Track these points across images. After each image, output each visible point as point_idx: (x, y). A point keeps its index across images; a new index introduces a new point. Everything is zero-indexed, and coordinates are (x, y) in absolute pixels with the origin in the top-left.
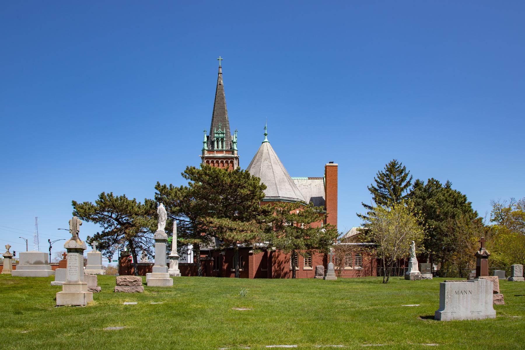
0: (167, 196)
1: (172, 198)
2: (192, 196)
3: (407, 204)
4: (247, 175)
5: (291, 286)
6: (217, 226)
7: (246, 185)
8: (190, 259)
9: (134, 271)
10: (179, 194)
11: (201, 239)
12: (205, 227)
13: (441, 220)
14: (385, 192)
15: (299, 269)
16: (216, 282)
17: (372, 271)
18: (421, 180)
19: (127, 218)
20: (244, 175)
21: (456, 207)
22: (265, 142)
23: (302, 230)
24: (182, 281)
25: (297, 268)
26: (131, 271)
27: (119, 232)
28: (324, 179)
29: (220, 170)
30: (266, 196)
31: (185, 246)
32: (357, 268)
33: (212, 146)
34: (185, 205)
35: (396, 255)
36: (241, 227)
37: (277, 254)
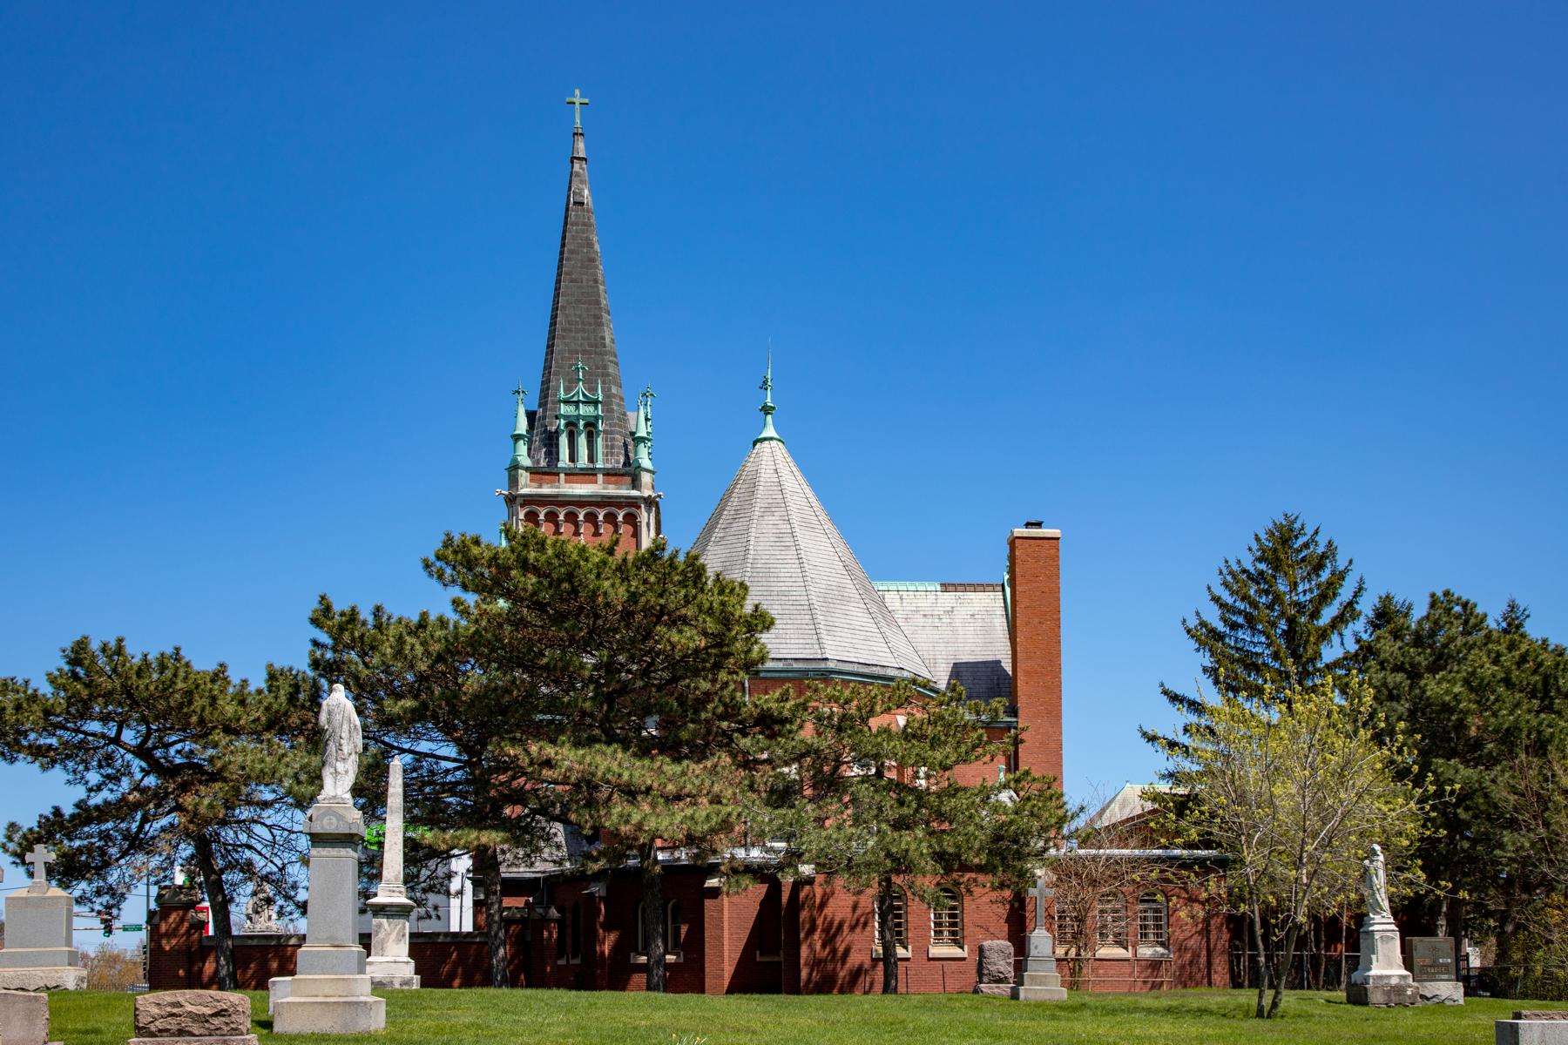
0: (362, 655)
1: (384, 663)
2: (468, 654)
3: (1347, 694)
4: (694, 572)
5: (878, 1027)
6: (573, 779)
7: (690, 611)
8: (460, 916)
9: (217, 972)
10: (413, 646)
11: (505, 830)
12: (522, 780)
13: (1491, 762)
14: (1255, 645)
15: (909, 955)
16: (570, 1009)
17: (1209, 964)
18: (1399, 599)
19: (188, 746)
20: (683, 573)
21: (1548, 708)
22: (765, 439)
23: (920, 795)
24: (425, 1008)
25: (900, 952)
26: (201, 971)
27: (151, 805)
28: (1003, 590)
29: (583, 550)
30: (772, 656)
31: (436, 860)
32: (1146, 952)
33: (549, 454)
34: (437, 691)
35: (1306, 903)
36: (670, 780)
37: (819, 891)
